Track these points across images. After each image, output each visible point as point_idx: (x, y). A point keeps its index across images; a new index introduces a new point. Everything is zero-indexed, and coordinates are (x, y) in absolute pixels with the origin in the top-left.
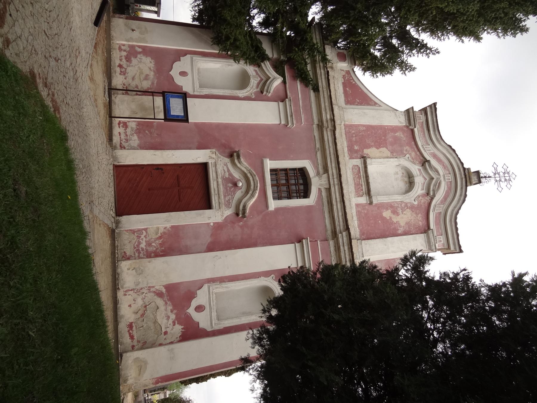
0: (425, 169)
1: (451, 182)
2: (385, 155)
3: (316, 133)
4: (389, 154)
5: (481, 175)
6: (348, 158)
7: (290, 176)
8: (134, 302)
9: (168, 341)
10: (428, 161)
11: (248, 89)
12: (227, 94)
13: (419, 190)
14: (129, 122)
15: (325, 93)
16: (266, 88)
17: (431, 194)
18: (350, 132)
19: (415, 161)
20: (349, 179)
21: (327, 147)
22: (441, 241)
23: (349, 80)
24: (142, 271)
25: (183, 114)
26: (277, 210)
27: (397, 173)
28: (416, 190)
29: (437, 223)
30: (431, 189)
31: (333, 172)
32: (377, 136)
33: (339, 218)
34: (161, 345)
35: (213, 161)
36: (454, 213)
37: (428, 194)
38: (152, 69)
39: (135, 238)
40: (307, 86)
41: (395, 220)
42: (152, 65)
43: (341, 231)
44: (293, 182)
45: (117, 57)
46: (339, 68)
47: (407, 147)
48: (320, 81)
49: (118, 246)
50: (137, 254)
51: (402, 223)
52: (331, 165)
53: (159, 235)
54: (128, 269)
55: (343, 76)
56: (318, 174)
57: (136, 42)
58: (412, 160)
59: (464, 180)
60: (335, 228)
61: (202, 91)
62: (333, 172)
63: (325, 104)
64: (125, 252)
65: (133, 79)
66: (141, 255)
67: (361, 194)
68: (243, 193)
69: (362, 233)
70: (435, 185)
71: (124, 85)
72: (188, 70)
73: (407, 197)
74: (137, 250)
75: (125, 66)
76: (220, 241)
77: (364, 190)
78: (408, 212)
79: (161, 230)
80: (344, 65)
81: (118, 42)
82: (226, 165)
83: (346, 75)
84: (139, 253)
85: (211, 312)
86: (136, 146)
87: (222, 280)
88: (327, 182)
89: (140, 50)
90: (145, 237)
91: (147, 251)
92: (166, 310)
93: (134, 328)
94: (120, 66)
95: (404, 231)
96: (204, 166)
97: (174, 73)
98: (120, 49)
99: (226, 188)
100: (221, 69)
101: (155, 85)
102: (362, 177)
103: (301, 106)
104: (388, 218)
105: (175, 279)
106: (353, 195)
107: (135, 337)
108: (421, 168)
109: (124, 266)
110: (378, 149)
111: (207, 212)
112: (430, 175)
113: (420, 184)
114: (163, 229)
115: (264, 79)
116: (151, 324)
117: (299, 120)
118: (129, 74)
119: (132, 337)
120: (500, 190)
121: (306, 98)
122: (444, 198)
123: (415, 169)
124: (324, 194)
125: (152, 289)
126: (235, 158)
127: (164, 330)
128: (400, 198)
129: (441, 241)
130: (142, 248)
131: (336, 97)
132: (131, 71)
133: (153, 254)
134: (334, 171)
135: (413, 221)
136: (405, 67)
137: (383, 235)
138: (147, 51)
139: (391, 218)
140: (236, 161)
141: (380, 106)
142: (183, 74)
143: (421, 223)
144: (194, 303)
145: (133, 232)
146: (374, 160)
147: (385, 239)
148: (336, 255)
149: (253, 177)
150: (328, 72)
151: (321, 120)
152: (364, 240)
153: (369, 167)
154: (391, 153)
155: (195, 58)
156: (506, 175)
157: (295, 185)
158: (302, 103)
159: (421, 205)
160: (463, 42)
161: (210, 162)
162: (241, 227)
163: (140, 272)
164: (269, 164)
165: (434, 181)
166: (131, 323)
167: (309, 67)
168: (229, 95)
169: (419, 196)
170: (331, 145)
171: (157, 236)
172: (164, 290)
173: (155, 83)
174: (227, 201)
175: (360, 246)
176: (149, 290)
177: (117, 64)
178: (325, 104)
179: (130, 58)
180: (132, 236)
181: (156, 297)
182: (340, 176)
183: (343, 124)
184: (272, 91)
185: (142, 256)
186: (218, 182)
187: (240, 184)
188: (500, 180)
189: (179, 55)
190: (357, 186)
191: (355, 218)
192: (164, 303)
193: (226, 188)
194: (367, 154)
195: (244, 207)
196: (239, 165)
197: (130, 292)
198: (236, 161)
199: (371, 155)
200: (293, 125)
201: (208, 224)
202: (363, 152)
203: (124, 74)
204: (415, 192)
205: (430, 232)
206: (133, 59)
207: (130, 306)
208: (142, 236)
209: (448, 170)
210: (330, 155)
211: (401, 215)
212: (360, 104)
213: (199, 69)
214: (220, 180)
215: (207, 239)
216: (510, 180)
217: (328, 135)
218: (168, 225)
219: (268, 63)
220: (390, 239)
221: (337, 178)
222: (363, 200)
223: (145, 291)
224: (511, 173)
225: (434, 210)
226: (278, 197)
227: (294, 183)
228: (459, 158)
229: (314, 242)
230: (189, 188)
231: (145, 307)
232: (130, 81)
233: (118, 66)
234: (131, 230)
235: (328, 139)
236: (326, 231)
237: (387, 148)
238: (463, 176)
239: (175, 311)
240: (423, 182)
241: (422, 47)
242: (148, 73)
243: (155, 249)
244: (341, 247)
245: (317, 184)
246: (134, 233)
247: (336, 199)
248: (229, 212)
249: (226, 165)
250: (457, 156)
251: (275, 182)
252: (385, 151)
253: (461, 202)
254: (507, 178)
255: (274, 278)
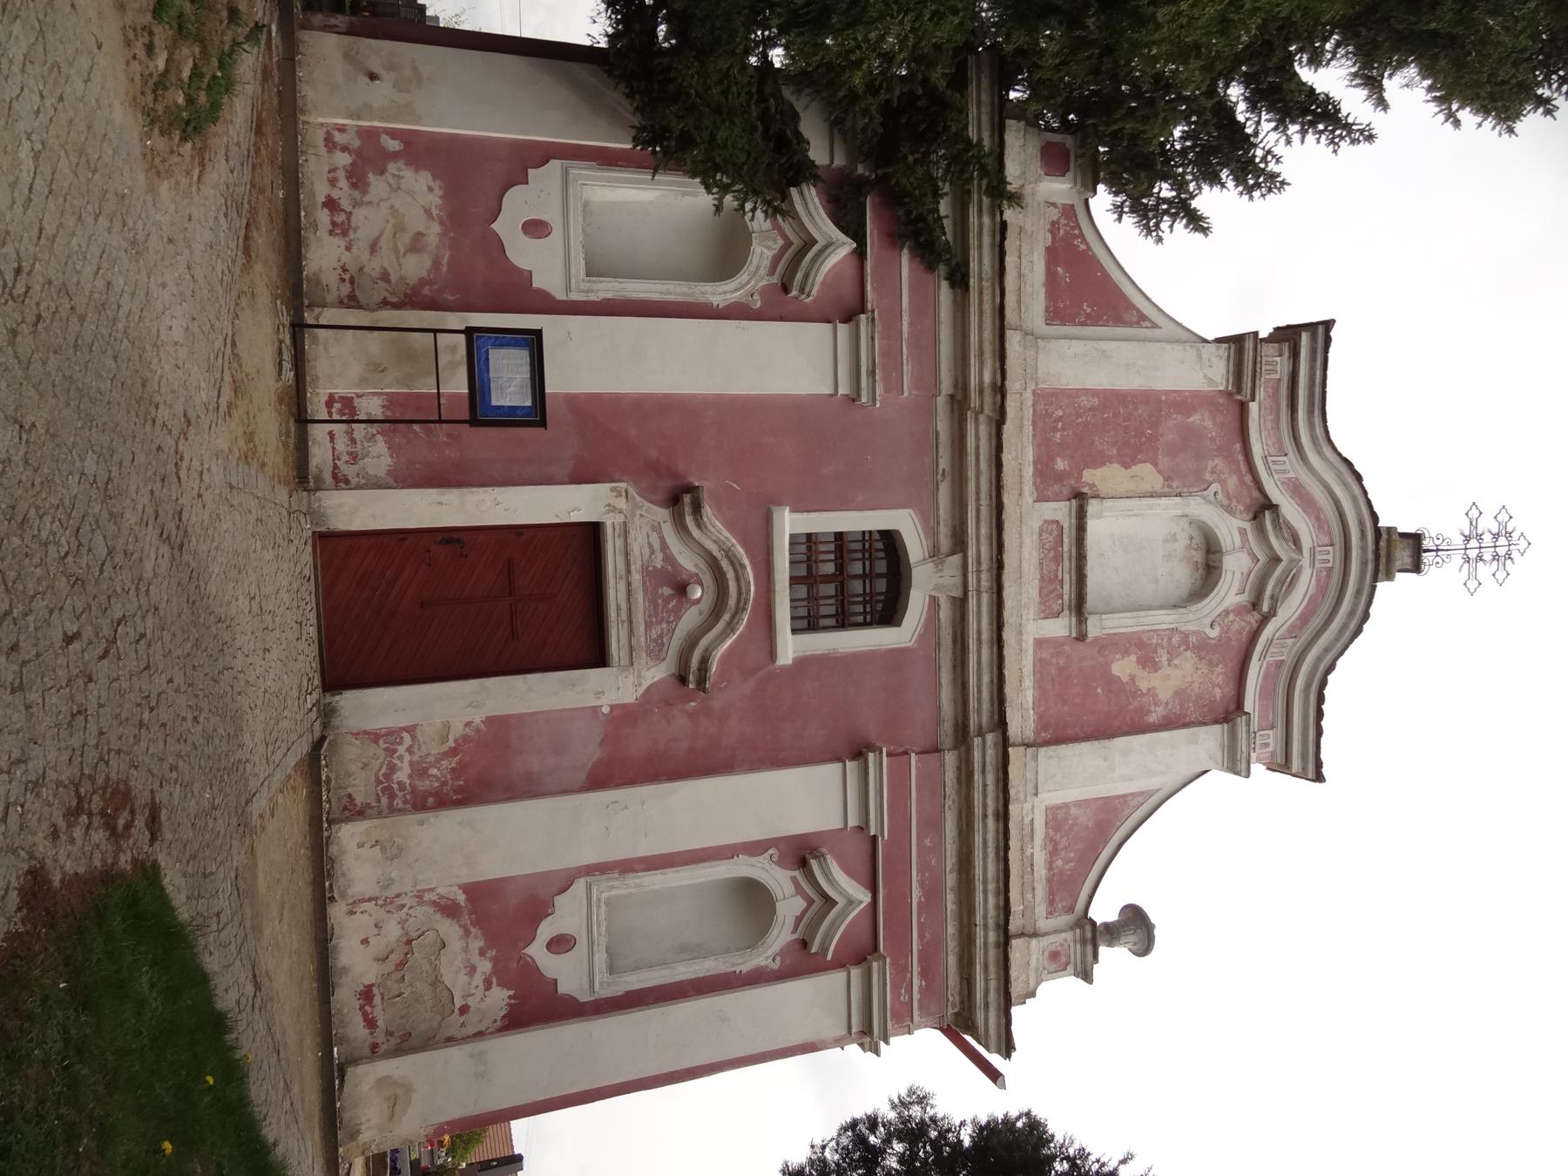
0: (1261, 531)
1: (1330, 570)
2: (1145, 487)
3: (943, 425)
4: (1157, 482)
5: (1427, 544)
6: (1030, 500)
7: (851, 551)
8: (376, 931)
9: (470, 1030)
10: (1273, 508)
11: (743, 277)
12: (672, 298)
13: (1229, 593)
14: (359, 396)
15: (987, 298)
16: (799, 276)
17: (1265, 608)
18: (1048, 415)
19: (1234, 503)
20: (1025, 565)
21: (971, 473)
22: (1267, 745)
23: (1069, 238)
24: (401, 850)
25: (528, 403)
26: (802, 663)
27: (1173, 538)
28: (1222, 593)
29: (1266, 694)
30: (1268, 593)
31: (978, 552)
32: (1127, 428)
33: (980, 691)
34: (450, 1041)
35: (620, 519)
36: (1322, 667)
37: (1255, 605)
38: (435, 212)
39: (381, 754)
40: (930, 267)
41: (1143, 685)
42: (434, 200)
43: (980, 728)
44: (857, 568)
45: (321, 172)
46: (1040, 197)
47: (1218, 461)
48: (974, 253)
49: (329, 780)
50: (384, 801)
51: (1164, 695)
52: (978, 529)
53: (451, 743)
54: (361, 845)
55: (1053, 223)
56: (934, 553)
57: (382, 119)
58: (1226, 502)
59: (1370, 567)
60: (966, 716)
61: (596, 286)
62: (978, 552)
63: (980, 333)
64: (350, 796)
65: (374, 247)
66: (398, 803)
67: (1056, 608)
68: (705, 616)
69: (1043, 724)
70: (1280, 582)
71: (345, 270)
72: (552, 216)
73: (1191, 617)
74: (384, 790)
75: (345, 204)
76: (627, 760)
77: (1066, 597)
78: (1188, 661)
79: (457, 730)
80: (1059, 189)
81: (321, 120)
82: (657, 529)
83: (1063, 221)
84: (392, 796)
85: (591, 954)
86: (382, 473)
87: (627, 867)
88: (958, 580)
89: (394, 145)
90: (409, 750)
91: (414, 789)
92: (466, 950)
93: (377, 1000)
94: (331, 204)
95: (1166, 718)
96: (593, 531)
97: (507, 226)
98: (330, 144)
99: (652, 598)
100: (661, 206)
101: (444, 269)
102: (1066, 556)
103: (905, 335)
104: (1125, 679)
105: (492, 867)
106: (1031, 613)
107: (380, 1023)
108: (1247, 525)
109: (349, 837)
110: (1126, 466)
111: (594, 675)
112: (1271, 547)
113: (1238, 575)
114: (461, 728)
115: (797, 242)
116: (424, 988)
117: (894, 385)
118: (360, 234)
119: (371, 1023)
120: (1472, 586)
121: (925, 309)
122: (1299, 618)
123: (1230, 529)
124: (945, 614)
125: (427, 897)
126: (688, 510)
127: (458, 1003)
128: (1169, 619)
129: (1267, 745)
130: (399, 783)
131: (1019, 301)
132: (368, 221)
133: (431, 800)
134: (984, 550)
135: (1196, 686)
136: (1254, 175)
137: (1103, 731)
138: (420, 150)
139: (1132, 679)
140: (689, 520)
141: (1155, 326)
142: (535, 228)
143: (1220, 692)
144: (546, 930)
145: (375, 737)
146: (1109, 503)
147: (1106, 743)
148: (959, 793)
149: (735, 570)
150: (1004, 225)
151: (961, 383)
152: (1047, 743)
153: (1092, 525)
154: (1166, 479)
155: (579, 170)
156: (1502, 541)
157: (863, 576)
158: (911, 324)
159: (1230, 639)
160: (1457, 123)
161: (611, 522)
162: (692, 716)
163: (392, 851)
164: (789, 523)
165: (1280, 569)
166: (370, 987)
167: (944, 207)
168: (679, 299)
169: (1227, 612)
170: (983, 466)
171: (445, 748)
172: (462, 898)
173: (445, 261)
174: (655, 640)
175: (1031, 765)
176: (420, 897)
177: (321, 199)
178: (980, 333)
179: (364, 175)
180: (372, 749)
181: (438, 916)
182: (1000, 566)
183: (1031, 386)
184: (814, 292)
185: (401, 805)
186: (629, 584)
187: (698, 593)
188: (1480, 558)
189: (523, 160)
190: (1049, 583)
191: (1028, 682)
192: (460, 932)
193: (654, 603)
194: (1092, 486)
195: (705, 661)
196: (695, 533)
197: (366, 906)
198: (689, 520)
199: (1103, 489)
200: (876, 396)
201: (595, 710)
202: (1080, 476)
203: (345, 233)
204: (1217, 600)
205: (1241, 722)
206: (371, 177)
207: (365, 942)
208: (401, 750)
209: (1330, 534)
210: (978, 499)
211: (1166, 670)
212: (1094, 320)
213: (586, 204)
214: (636, 577)
215: (588, 752)
216: (1509, 556)
217: (978, 435)
218: (478, 718)
219: (812, 193)
220: (1120, 742)
221: (990, 570)
222: (1059, 627)
223: (409, 901)
224: (1515, 536)
225: (1263, 656)
226: (807, 623)
227: (860, 580)
228: (1369, 503)
229: (899, 755)
230: (540, 603)
231: (409, 942)
232: (364, 256)
233: (325, 205)
234: (366, 733)
235: (977, 448)
236: (939, 722)
237: (1155, 465)
238: (1370, 556)
239: (491, 953)
240: (1245, 571)
241: (1319, 115)
242: (421, 229)
243: (436, 784)
244: (977, 776)
245: (928, 583)
246: (376, 741)
247: (979, 632)
248: (657, 673)
249: (657, 529)
250: (1365, 493)
251: (802, 571)
252: (1147, 474)
253: (1348, 634)
254: (1502, 551)
255: (775, 858)
